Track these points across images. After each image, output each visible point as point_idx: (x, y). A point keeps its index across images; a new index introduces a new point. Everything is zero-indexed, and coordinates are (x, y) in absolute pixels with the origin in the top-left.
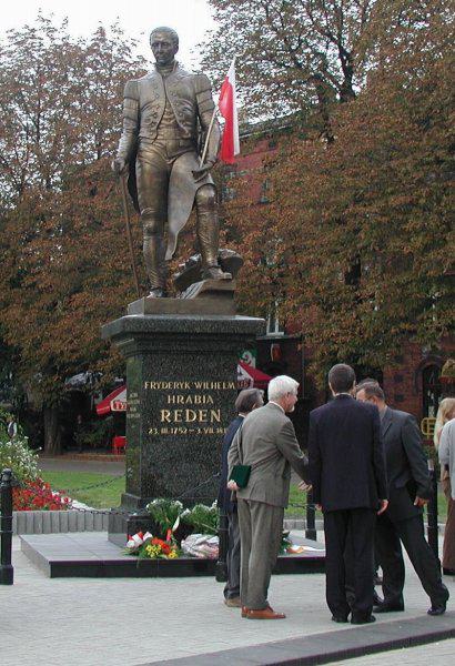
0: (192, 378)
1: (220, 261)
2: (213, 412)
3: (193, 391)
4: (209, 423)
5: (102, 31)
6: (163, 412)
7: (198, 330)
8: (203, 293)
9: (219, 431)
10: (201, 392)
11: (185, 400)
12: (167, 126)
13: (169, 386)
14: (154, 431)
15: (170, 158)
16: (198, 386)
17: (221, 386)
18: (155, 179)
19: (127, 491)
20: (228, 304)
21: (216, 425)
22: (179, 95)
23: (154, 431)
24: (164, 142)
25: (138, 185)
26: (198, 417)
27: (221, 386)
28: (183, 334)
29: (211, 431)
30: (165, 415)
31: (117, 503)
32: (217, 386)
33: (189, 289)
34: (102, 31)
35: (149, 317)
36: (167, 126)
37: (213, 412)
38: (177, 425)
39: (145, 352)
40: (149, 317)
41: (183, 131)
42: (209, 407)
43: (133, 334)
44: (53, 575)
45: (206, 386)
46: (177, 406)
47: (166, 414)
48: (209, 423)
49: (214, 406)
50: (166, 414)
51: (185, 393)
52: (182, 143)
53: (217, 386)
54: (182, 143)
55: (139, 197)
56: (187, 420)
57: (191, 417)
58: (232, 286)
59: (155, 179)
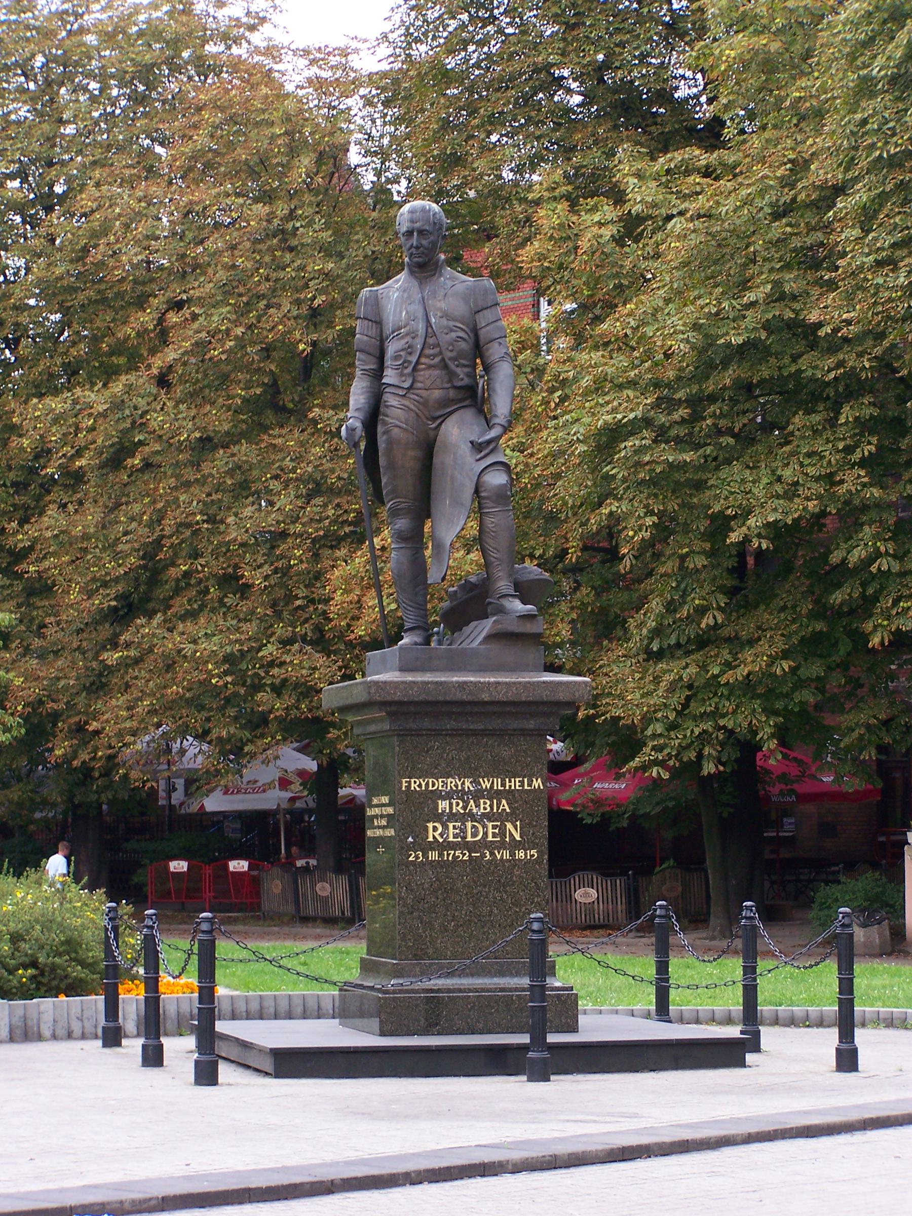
0: (474, 773)
1: (517, 586)
2: (509, 826)
3: (478, 795)
4: (503, 841)
5: (472, 442)
6: (430, 825)
7: (485, 697)
8: (495, 637)
9: (521, 854)
10: (493, 794)
11: (465, 808)
12: (430, 367)
13: (439, 784)
14: (417, 857)
15: (434, 419)
16: (486, 784)
17: (522, 785)
18: (411, 453)
19: (369, 952)
20: (535, 655)
21: (515, 845)
22: (447, 316)
23: (417, 857)
24: (424, 393)
25: (382, 461)
26: (485, 834)
27: (522, 785)
28: (462, 703)
29: (506, 855)
30: (434, 831)
31: (353, 974)
32: (514, 784)
33: (467, 630)
34: (472, 442)
35: (409, 678)
36: (430, 367)
37: (509, 826)
38: (453, 846)
39: (403, 734)
40: (409, 678)
41: (456, 375)
42: (501, 817)
43: (384, 704)
44: (279, 1074)
45: (498, 785)
46: (453, 816)
47: (435, 829)
48: (503, 841)
49: (512, 817)
50: (435, 829)
51: (462, 794)
52: (452, 393)
53: (514, 784)
54: (452, 393)
55: (384, 480)
56: (469, 839)
57: (474, 835)
58: (538, 626)
59: (411, 453)
